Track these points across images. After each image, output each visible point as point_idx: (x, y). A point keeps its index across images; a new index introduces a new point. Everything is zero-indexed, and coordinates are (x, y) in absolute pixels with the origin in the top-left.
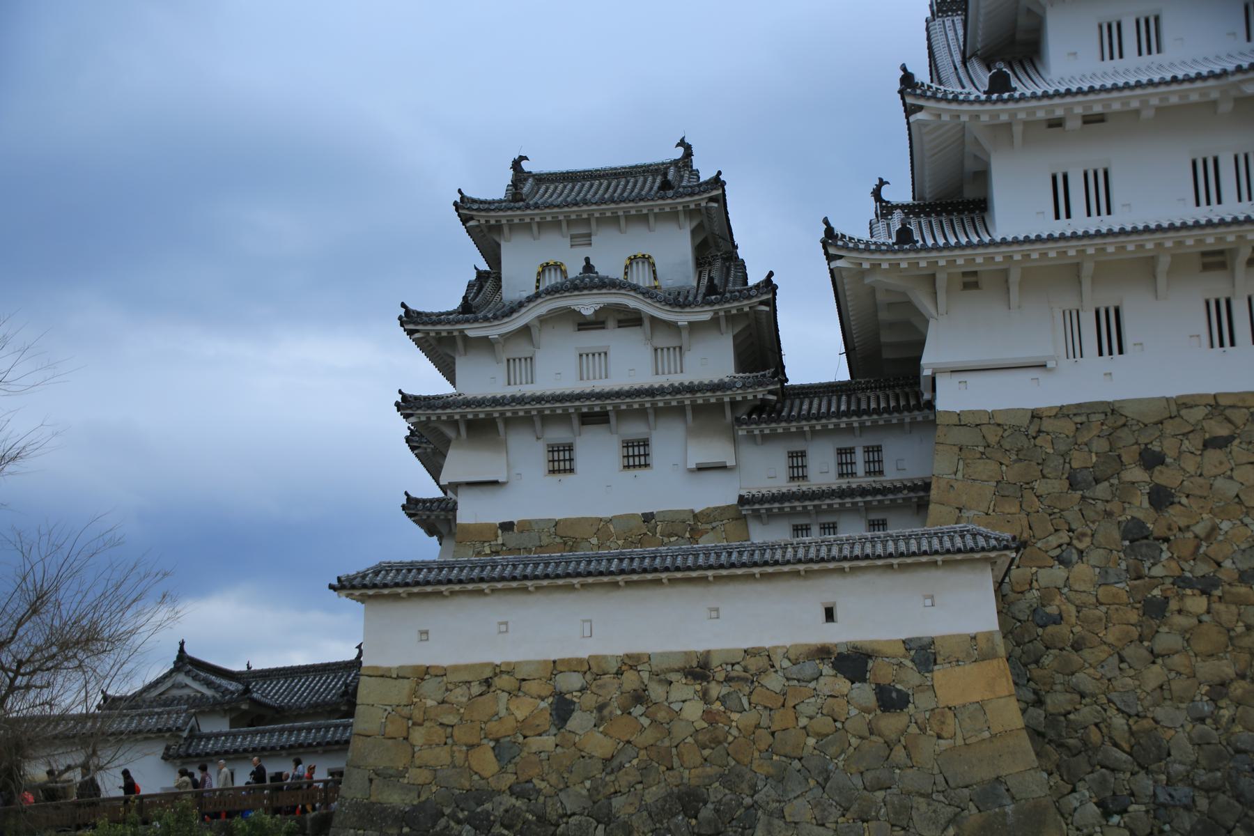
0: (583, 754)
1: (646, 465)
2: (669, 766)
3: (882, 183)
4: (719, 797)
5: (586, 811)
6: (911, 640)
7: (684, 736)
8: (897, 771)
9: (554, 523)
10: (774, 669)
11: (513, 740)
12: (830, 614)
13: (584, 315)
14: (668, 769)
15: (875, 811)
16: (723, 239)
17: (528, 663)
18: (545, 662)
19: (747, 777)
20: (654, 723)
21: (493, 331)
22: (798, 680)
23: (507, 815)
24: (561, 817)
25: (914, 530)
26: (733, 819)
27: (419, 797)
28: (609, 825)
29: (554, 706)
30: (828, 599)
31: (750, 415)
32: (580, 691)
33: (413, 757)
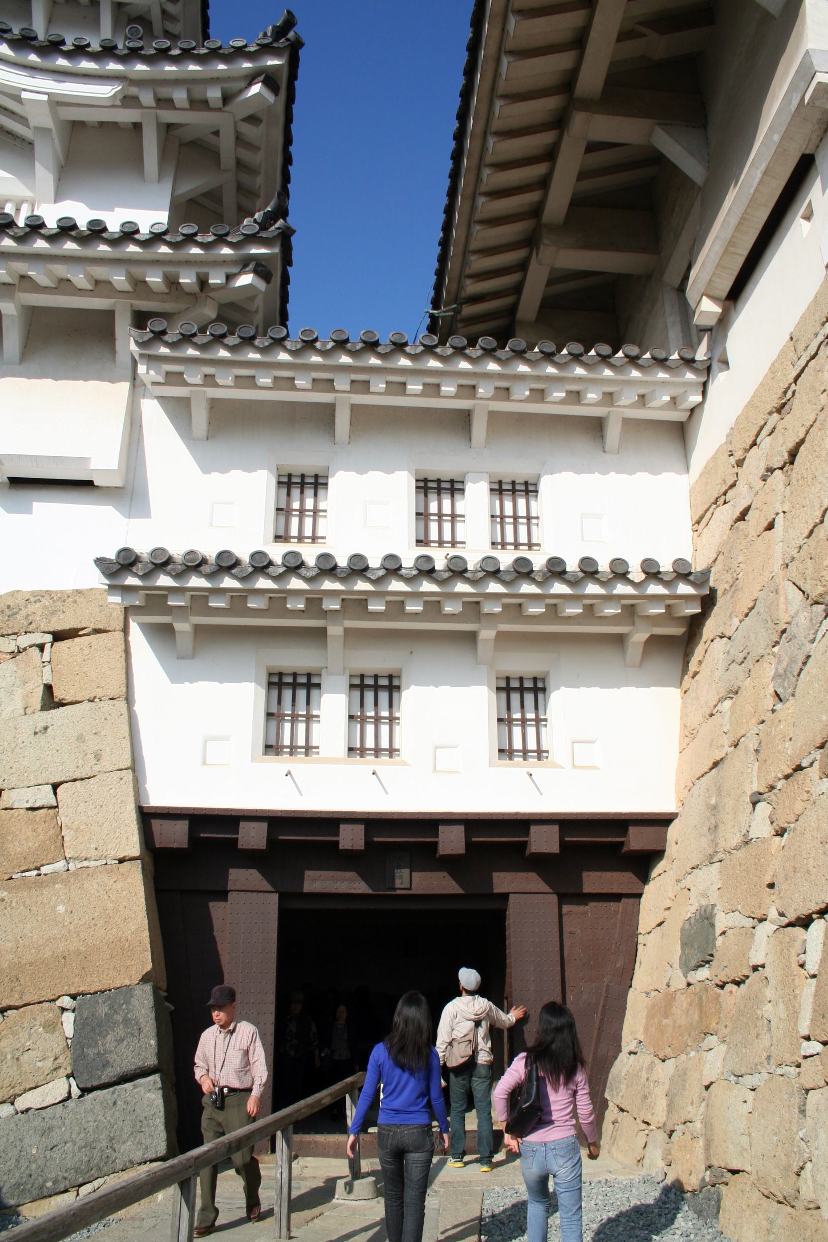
1: (392, 751)
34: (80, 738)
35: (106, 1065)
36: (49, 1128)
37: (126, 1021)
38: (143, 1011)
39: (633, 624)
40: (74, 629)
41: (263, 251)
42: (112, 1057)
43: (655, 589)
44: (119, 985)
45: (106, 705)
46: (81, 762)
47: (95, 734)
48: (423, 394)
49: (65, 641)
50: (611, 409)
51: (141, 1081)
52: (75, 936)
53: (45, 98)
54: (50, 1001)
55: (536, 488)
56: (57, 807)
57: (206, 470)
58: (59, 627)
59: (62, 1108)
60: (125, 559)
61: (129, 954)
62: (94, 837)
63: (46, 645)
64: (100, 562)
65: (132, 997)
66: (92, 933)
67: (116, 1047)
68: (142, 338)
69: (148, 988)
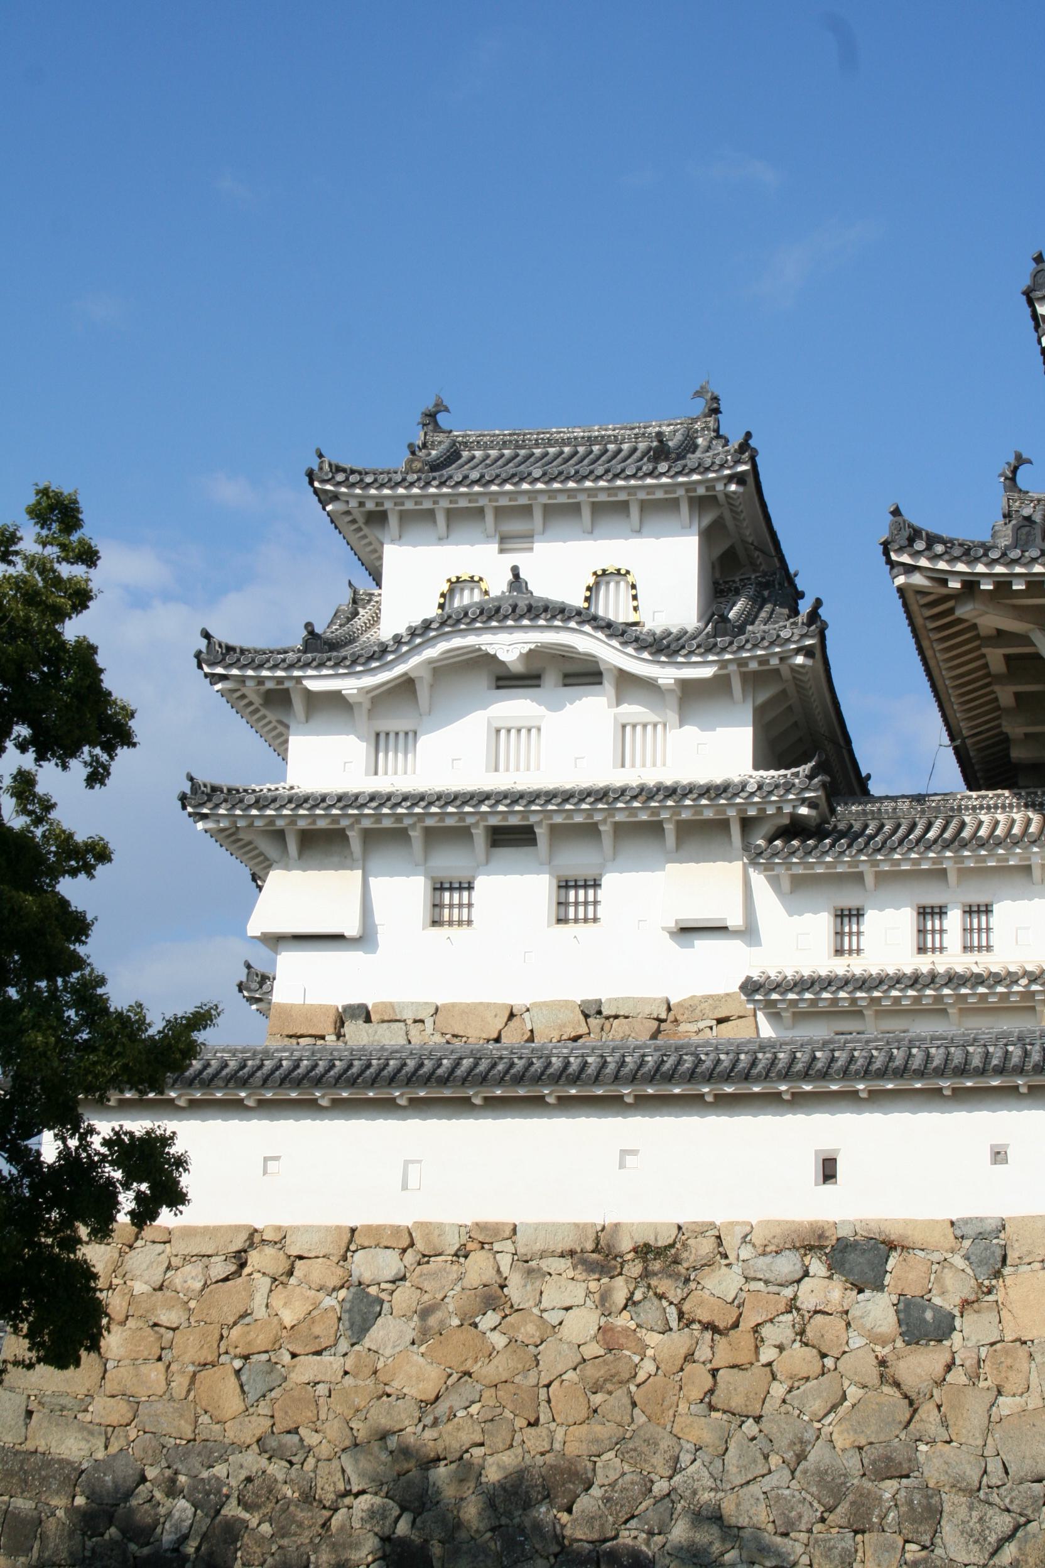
0: (388, 1390)
1: (595, 920)
2: (532, 1420)
3: (1020, 461)
4: (612, 1478)
5: (385, 1488)
6: (966, 1221)
7: (560, 1368)
8: (923, 1448)
9: (432, 1011)
10: (727, 1262)
11: (274, 1360)
12: (828, 1171)
13: (503, 663)
14: (530, 1424)
15: (878, 1516)
16: (762, 551)
17: (307, 1229)
18: (338, 1228)
19: (663, 1445)
20: (513, 1343)
21: (349, 685)
22: (766, 1282)
23: (250, 1486)
24: (347, 1493)
25: (970, 1025)
26: (633, 1517)
27: (106, 1447)
28: (420, 1514)
29: (347, 1306)
30: (828, 1145)
31: (771, 841)
32: (393, 1282)
33: (103, 1378)
41: (812, 794)
53: (672, 681)
57: (791, 914)
58: (720, 1016)
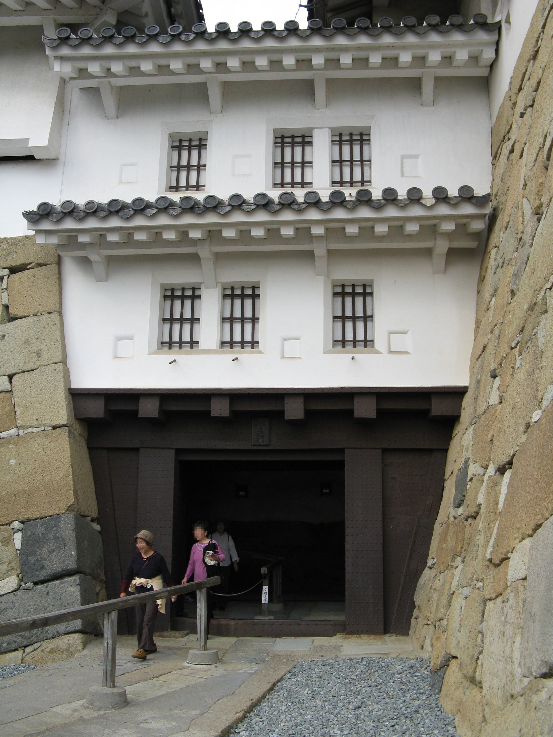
34: (27, 342)
35: (43, 567)
36: (4, 609)
37: (56, 538)
38: (67, 532)
39: (435, 239)
40: (23, 264)
42: (45, 563)
43: (444, 210)
44: (51, 514)
45: (45, 318)
46: (27, 359)
47: (37, 338)
48: (411, 66)
49: (17, 274)
50: (422, 70)
51: (67, 579)
52: (22, 480)
54: (6, 524)
55: (369, 137)
56: (11, 391)
58: (14, 264)
59: (13, 596)
60: (43, 211)
61: (58, 492)
62: (36, 411)
63: (5, 277)
64: (28, 215)
65: (59, 522)
66: (33, 478)
67: (48, 556)
68: (52, 44)
69: (71, 516)
